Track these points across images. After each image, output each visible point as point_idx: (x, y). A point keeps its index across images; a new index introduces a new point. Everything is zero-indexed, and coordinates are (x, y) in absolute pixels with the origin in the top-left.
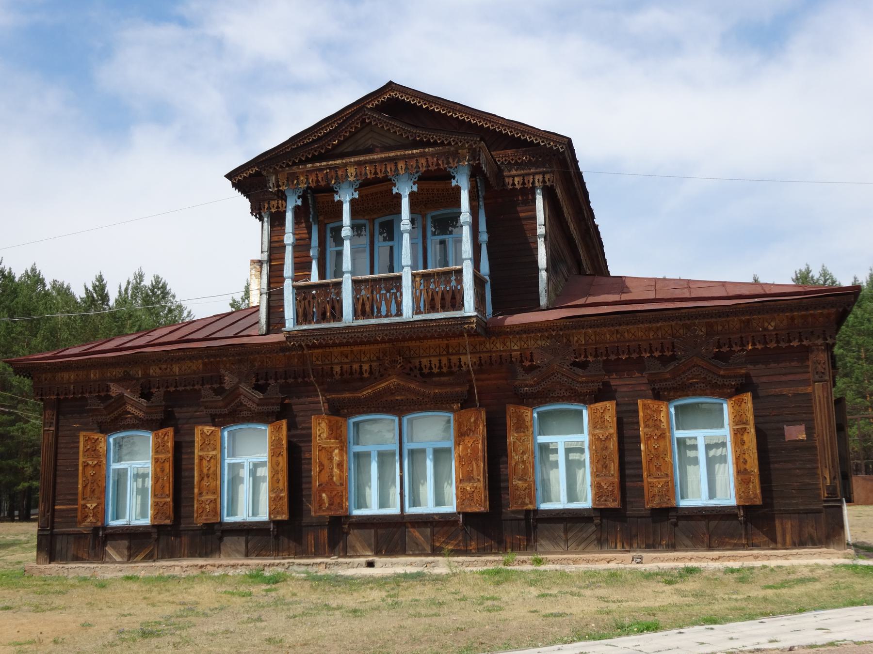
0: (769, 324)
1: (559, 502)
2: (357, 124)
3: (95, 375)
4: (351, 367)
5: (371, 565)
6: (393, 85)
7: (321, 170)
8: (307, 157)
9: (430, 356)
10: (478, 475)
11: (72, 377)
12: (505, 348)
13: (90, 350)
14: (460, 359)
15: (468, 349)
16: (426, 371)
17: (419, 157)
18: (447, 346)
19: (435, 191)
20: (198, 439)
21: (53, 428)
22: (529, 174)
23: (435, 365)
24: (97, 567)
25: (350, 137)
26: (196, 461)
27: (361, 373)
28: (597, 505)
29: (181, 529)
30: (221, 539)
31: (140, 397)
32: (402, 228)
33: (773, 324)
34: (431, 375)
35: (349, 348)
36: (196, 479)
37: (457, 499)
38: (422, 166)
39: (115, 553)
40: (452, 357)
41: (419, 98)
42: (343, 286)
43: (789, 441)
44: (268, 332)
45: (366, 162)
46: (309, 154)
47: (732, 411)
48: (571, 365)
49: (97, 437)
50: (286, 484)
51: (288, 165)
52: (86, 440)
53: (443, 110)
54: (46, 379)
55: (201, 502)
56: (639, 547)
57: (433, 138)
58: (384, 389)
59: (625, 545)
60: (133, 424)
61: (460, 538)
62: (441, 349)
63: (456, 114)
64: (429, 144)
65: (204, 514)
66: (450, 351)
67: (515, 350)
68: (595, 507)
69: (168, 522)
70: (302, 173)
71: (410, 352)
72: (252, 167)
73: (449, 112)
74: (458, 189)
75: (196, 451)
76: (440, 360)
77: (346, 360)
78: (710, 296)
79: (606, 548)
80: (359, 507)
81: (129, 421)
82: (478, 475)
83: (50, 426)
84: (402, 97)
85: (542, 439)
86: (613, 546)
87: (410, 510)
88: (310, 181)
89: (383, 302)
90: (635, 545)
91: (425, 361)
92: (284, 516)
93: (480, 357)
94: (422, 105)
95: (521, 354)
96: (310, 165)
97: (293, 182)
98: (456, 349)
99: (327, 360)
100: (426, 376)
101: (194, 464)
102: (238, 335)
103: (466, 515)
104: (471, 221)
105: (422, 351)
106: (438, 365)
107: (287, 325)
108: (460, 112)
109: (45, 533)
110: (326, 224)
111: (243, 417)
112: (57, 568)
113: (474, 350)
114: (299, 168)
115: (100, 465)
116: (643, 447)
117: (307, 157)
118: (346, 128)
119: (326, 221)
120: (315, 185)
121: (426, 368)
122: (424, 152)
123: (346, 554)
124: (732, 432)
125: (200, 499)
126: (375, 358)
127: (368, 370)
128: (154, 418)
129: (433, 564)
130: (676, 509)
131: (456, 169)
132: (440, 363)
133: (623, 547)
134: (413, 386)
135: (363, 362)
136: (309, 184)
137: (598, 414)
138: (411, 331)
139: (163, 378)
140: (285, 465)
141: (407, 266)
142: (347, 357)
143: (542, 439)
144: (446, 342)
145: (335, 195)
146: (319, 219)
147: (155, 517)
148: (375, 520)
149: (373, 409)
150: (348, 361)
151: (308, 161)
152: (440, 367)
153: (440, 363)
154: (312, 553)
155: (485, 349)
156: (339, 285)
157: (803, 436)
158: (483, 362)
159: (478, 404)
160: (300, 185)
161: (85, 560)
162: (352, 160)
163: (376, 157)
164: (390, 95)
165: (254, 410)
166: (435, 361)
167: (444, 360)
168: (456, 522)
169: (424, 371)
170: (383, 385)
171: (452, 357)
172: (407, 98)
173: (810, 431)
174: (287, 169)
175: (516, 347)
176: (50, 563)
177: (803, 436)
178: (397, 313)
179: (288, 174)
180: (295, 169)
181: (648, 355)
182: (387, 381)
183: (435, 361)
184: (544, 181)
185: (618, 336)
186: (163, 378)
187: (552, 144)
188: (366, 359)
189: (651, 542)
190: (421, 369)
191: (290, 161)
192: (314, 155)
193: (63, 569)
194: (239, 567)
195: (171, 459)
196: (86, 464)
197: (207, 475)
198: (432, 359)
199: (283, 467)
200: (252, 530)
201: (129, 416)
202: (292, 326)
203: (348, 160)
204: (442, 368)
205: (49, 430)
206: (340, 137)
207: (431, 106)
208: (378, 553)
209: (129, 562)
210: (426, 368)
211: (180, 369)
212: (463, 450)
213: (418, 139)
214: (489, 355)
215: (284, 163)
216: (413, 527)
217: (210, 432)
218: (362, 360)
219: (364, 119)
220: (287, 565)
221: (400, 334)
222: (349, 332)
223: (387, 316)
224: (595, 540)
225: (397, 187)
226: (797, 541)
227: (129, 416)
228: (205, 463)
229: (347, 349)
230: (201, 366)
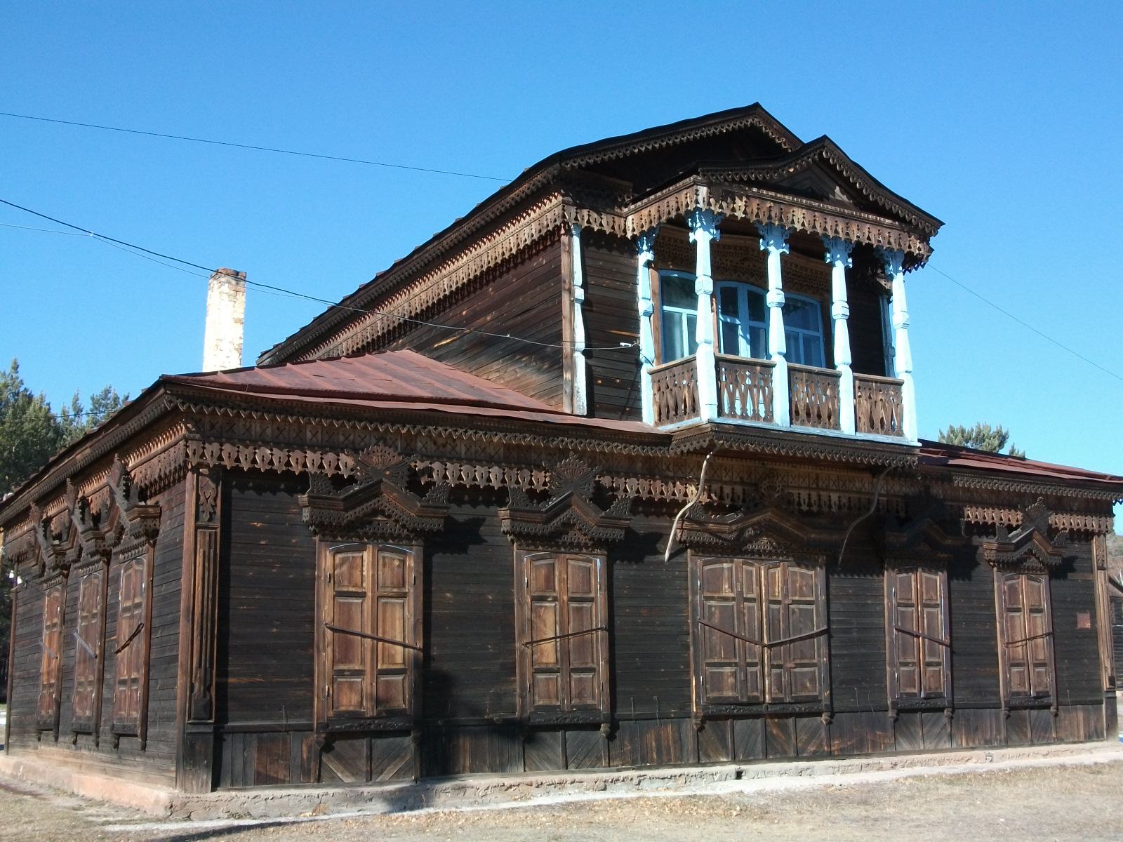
13: (194, 378)
14: (830, 497)
16: (805, 508)
19: (672, 240)
24: (327, 794)
39: (341, 768)
40: (822, 493)
43: (1081, 629)
76: (809, 495)
93: (849, 498)
95: (887, 501)
96: (755, 190)
98: (826, 482)
99: (680, 472)
106: (807, 501)
109: (202, 729)
112: (243, 799)
126: (738, 480)
129: (809, 771)
132: (809, 499)
133: (967, 744)
152: (810, 505)
153: (809, 499)
154: (652, 761)
155: (854, 489)
158: (852, 504)
161: (283, 781)
176: (213, 790)
178: (742, 414)
183: (804, 494)
188: (728, 479)
193: (256, 800)
194: (568, 785)
198: (842, 495)
209: (370, 783)
211: (468, 450)
218: (724, 479)
220: (636, 781)
230: (502, 450)
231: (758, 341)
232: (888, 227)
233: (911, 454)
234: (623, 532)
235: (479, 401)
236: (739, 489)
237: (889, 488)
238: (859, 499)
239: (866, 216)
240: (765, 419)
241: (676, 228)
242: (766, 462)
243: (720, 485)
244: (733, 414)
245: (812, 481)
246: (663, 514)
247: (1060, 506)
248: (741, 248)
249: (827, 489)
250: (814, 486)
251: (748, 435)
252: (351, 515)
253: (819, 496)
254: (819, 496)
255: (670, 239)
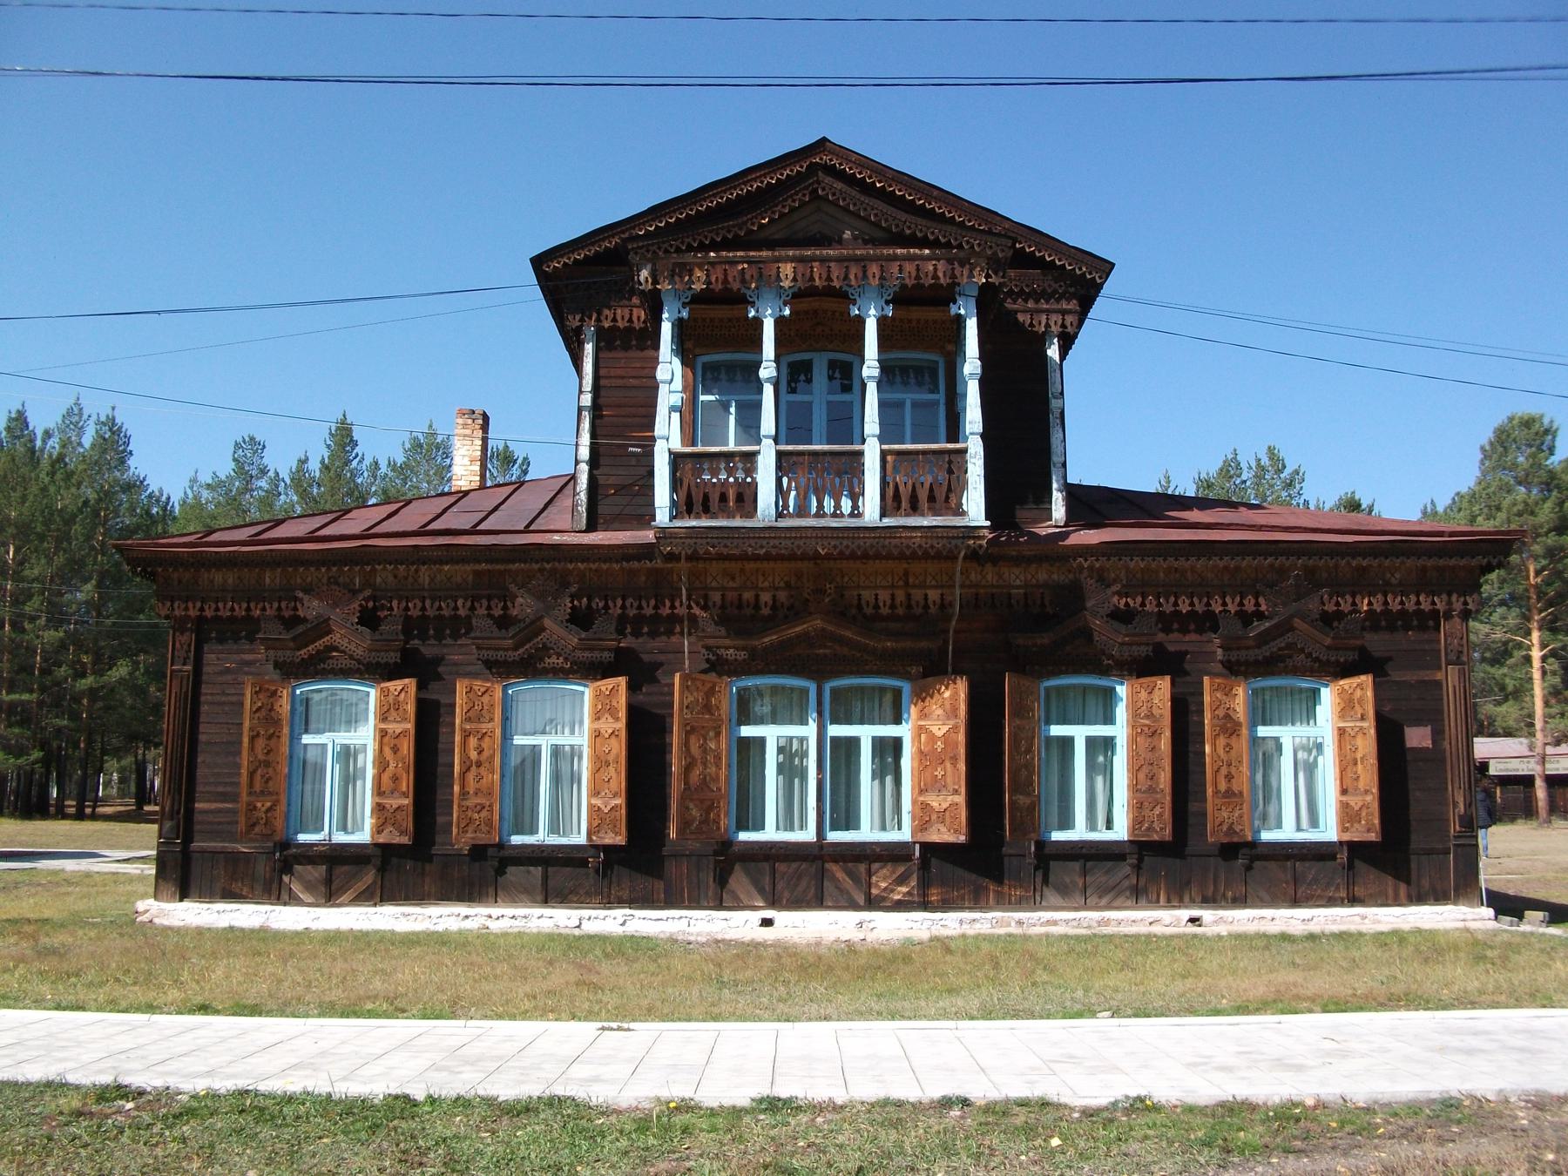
0: (1393, 575)
1: (1286, 830)
2: (804, 195)
3: (272, 581)
4: (740, 595)
5: (767, 923)
6: (828, 143)
7: (733, 263)
8: (713, 240)
9: (876, 587)
10: (954, 784)
11: (230, 581)
12: (1001, 582)
15: (957, 580)
16: (869, 611)
17: (904, 260)
18: (906, 573)
19: (837, 314)
20: (460, 699)
21: (189, 668)
22: (1042, 311)
23: (885, 602)
25: (852, 213)
26: (457, 738)
27: (757, 606)
28: (1135, 835)
29: (433, 852)
30: (500, 871)
31: (357, 623)
32: (866, 372)
33: (1397, 576)
34: (877, 617)
35: (739, 565)
36: (457, 769)
37: (913, 821)
38: (910, 277)
40: (913, 591)
41: (871, 170)
42: (760, 458)
44: (591, 527)
45: (813, 259)
46: (717, 234)
47: (1338, 700)
48: (1107, 616)
49: (274, 688)
50: (623, 784)
51: (678, 250)
52: (256, 692)
53: (910, 195)
54: (180, 582)
55: (464, 809)
56: (1193, 901)
57: (933, 233)
58: (798, 636)
59: (1172, 897)
60: (341, 669)
61: (914, 883)
62: (944, 576)
63: (930, 204)
64: (923, 243)
65: (470, 829)
66: (911, 580)
67: (1018, 587)
68: (1131, 839)
69: (405, 840)
70: (700, 266)
71: (843, 577)
72: (579, 249)
73: (920, 199)
74: (960, 322)
75: (458, 721)
76: (893, 595)
77: (731, 584)
78: (401, 530)
79: (1143, 902)
80: (743, 825)
81: (553, 661)
82: (954, 784)
83: (184, 664)
84: (841, 164)
85: (1057, 730)
86: (1155, 897)
87: (834, 836)
88: (713, 280)
89: (793, 493)
90: (1186, 898)
91: (867, 595)
92: (619, 838)
94: (874, 183)
95: (1025, 594)
97: (682, 277)
99: (697, 582)
100: (868, 619)
101: (454, 743)
102: (430, 527)
103: (927, 847)
104: (979, 371)
105: (863, 578)
106: (889, 602)
107: (658, 518)
108: (936, 199)
110: (695, 356)
111: (324, 669)
113: (968, 583)
114: (695, 256)
115: (279, 737)
116: (1208, 749)
117: (713, 240)
118: (785, 200)
119: (697, 351)
120: (720, 286)
121: (918, 606)
122: (868, 253)
123: (721, 903)
124: (1336, 732)
125: (464, 803)
126: (782, 584)
127: (770, 603)
128: (383, 661)
130: (1254, 844)
131: (756, 292)
134: (848, 634)
135: (762, 589)
136: (711, 283)
137: (391, 699)
138: (841, 544)
139: (401, 593)
140: (624, 753)
141: (874, 436)
142: (733, 579)
143: (1057, 730)
144: (906, 566)
145: (851, 306)
146: (685, 347)
147: (378, 829)
148: (773, 850)
149: (773, 668)
150: (735, 585)
151: (715, 246)
152: (893, 607)
156: (750, 457)
157: (1428, 743)
159: (950, 669)
160: (694, 283)
162: (791, 253)
163: (831, 252)
164: (821, 159)
165: (736, 660)
166: (884, 596)
167: (900, 596)
168: (908, 858)
169: (762, 612)
170: (797, 629)
171: (913, 591)
172: (850, 169)
173: (1438, 734)
174: (675, 255)
175: (1018, 582)
177: (1428, 743)
178: (852, 512)
179: (674, 263)
180: (689, 258)
181: (1221, 609)
182: (804, 623)
184: (1063, 326)
185: (1177, 575)
186: (401, 593)
187: (1084, 269)
188: (766, 584)
189: (1210, 893)
190: (859, 607)
191: (682, 243)
192: (724, 238)
195: (412, 732)
196: (255, 733)
197: (477, 763)
199: (618, 756)
200: (558, 859)
201: (334, 654)
202: (667, 519)
203: (783, 253)
204: (896, 608)
205: (181, 671)
206: (774, 213)
207: (890, 186)
208: (774, 902)
210: (918, 606)
212: (927, 743)
213: (908, 232)
214: (973, 590)
215: (671, 246)
216: (836, 861)
217: (483, 690)
218: (760, 585)
219: (816, 190)
221: (859, 547)
222: (770, 538)
223: (817, 515)
224: (1127, 888)
225: (857, 305)
226: (1414, 894)
227: (334, 654)
228: (473, 742)
229: (734, 566)
231: (846, 424)
232: (928, 258)
233: (973, 538)
234: (399, 655)
235: (447, 530)
236: (782, 596)
237: (1029, 577)
238: (977, 594)
239: (891, 251)
240: (852, 515)
241: (698, 306)
242: (819, 561)
243: (939, 591)
244: (820, 514)
245: (897, 578)
246: (660, 634)
247: (1361, 583)
248: (807, 312)
249: (923, 586)
250: (901, 583)
251: (707, 538)
252: (1265, 651)
253: (909, 596)
254: (909, 596)
255: (704, 320)
